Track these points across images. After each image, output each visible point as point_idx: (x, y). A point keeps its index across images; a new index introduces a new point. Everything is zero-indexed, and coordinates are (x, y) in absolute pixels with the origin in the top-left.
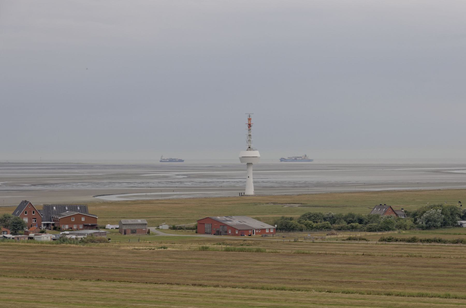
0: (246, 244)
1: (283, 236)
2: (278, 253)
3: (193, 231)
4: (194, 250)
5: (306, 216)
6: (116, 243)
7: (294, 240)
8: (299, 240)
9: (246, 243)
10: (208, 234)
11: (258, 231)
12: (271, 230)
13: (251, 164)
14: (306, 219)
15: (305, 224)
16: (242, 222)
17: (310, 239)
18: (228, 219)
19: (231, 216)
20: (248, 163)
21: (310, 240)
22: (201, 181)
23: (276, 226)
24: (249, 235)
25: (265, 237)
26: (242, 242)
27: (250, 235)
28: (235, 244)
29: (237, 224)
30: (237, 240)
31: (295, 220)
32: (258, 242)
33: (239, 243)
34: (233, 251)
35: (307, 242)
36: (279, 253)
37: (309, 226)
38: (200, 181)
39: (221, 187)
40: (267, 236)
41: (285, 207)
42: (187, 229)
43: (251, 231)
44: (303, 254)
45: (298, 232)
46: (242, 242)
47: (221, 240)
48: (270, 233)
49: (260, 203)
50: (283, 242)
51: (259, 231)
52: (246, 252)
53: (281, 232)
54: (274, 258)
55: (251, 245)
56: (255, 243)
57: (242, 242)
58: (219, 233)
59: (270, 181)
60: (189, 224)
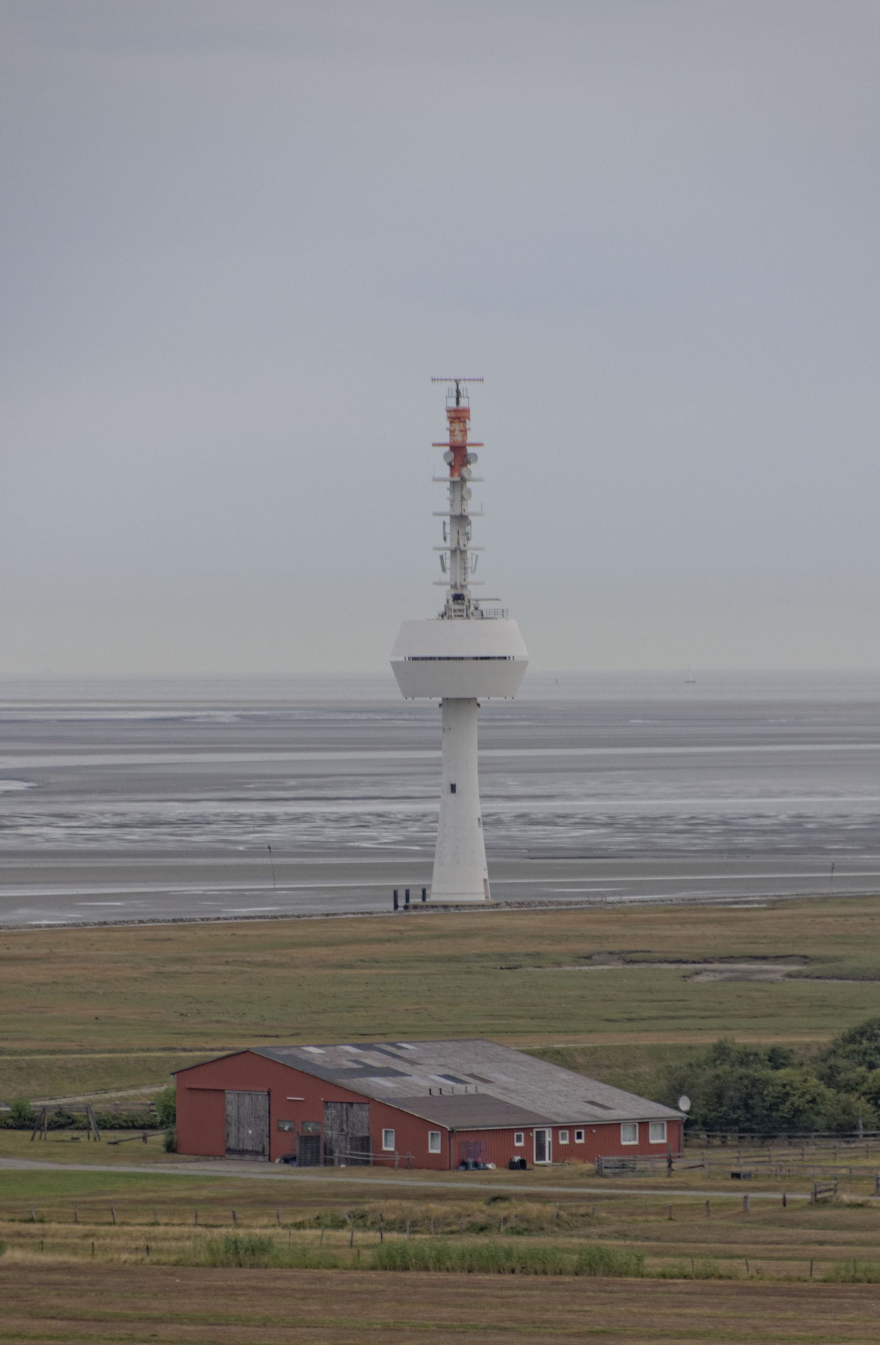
0: (505, 1220)
1: (735, 1170)
2: (720, 1277)
3: (144, 1138)
4: (177, 1263)
5: (869, 1039)
6: (239, 1222)
7: (808, 1197)
8: (846, 1197)
10: (248, 1157)
11: (571, 1139)
12: (651, 1130)
13: (471, 702)
14: (868, 1058)
15: (864, 1094)
16: (464, 1078)
18: (373, 1059)
20: (446, 700)
22: (123, 814)
23: (685, 1104)
24: (513, 1166)
25: (616, 1175)
26: (482, 1212)
27: (522, 1165)
28: (438, 1224)
29: (436, 1093)
30: (440, 1197)
31: (801, 1064)
32: (582, 1210)
33: (459, 1216)
34: (431, 1265)
38: (116, 814)
40: (633, 1170)
41: (699, 978)
42: (105, 1128)
43: (528, 1139)
45: (824, 1143)
46: (482, 1212)
47: (336, 1195)
48: (644, 1148)
50: (741, 1209)
51: (579, 1136)
52: (513, 1271)
53: (717, 1142)
54: (706, 1311)
55: (542, 1229)
56: (562, 1213)
57: (480, 1211)
60: (114, 1095)
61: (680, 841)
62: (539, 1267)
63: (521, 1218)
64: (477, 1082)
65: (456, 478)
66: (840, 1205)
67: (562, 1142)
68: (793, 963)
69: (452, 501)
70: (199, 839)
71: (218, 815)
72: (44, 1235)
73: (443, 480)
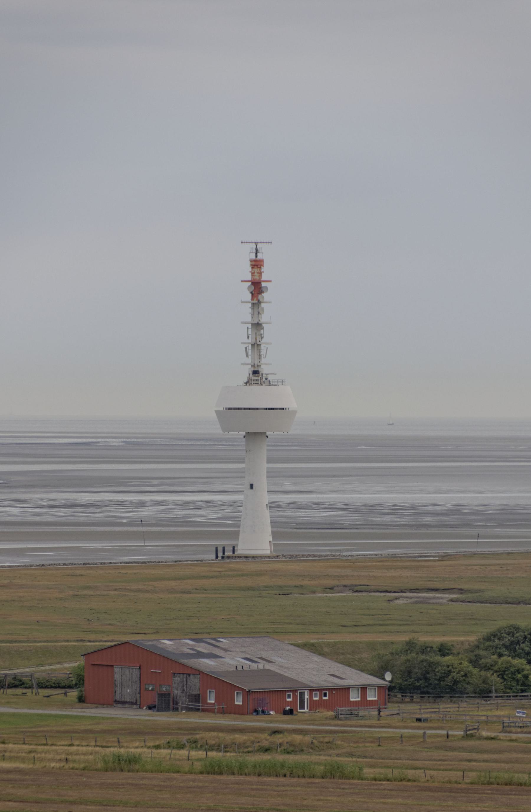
0: (281, 745)
1: (418, 716)
2: (409, 780)
4: (84, 769)
5: (499, 639)
7: (462, 733)
8: (484, 734)
9: (280, 741)
11: (320, 697)
13: (263, 435)
15: (496, 672)
16: (256, 660)
17: (525, 730)
18: (202, 648)
19: (214, 639)
20: (248, 433)
21: (526, 733)
23: (388, 676)
24: (285, 713)
26: (266, 740)
28: (240, 747)
29: (239, 668)
31: (459, 654)
32: (327, 740)
33: (253, 742)
34: (236, 772)
35: (511, 740)
36: (415, 784)
37: (514, 678)
38: (51, 500)
39: (142, 523)
41: (397, 602)
42: (42, 687)
43: (295, 697)
44: (507, 788)
45: (472, 701)
46: (266, 740)
47: (180, 729)
48: (364, 702)
49: (301, 586)
50: (421, 740)
51: (325, 695)
53: (407, 699)
54: (400, 800)
55: (302, 750)
56: (314, 741)
57: (265, 739)
58: (169, 704)
59: (323, 503)
60: (47, 667)
61: (387, 519)
62: (300, 774)
63: (290, 744)
64: (264, 662)
65: (255, 301)
66: (481, 738)
67: (315, 699)
68: (454, 593)
69: (253, 315)
70: (99, 515)
71: (111, 501)
72: (5, 751)
73: (247, 302)
